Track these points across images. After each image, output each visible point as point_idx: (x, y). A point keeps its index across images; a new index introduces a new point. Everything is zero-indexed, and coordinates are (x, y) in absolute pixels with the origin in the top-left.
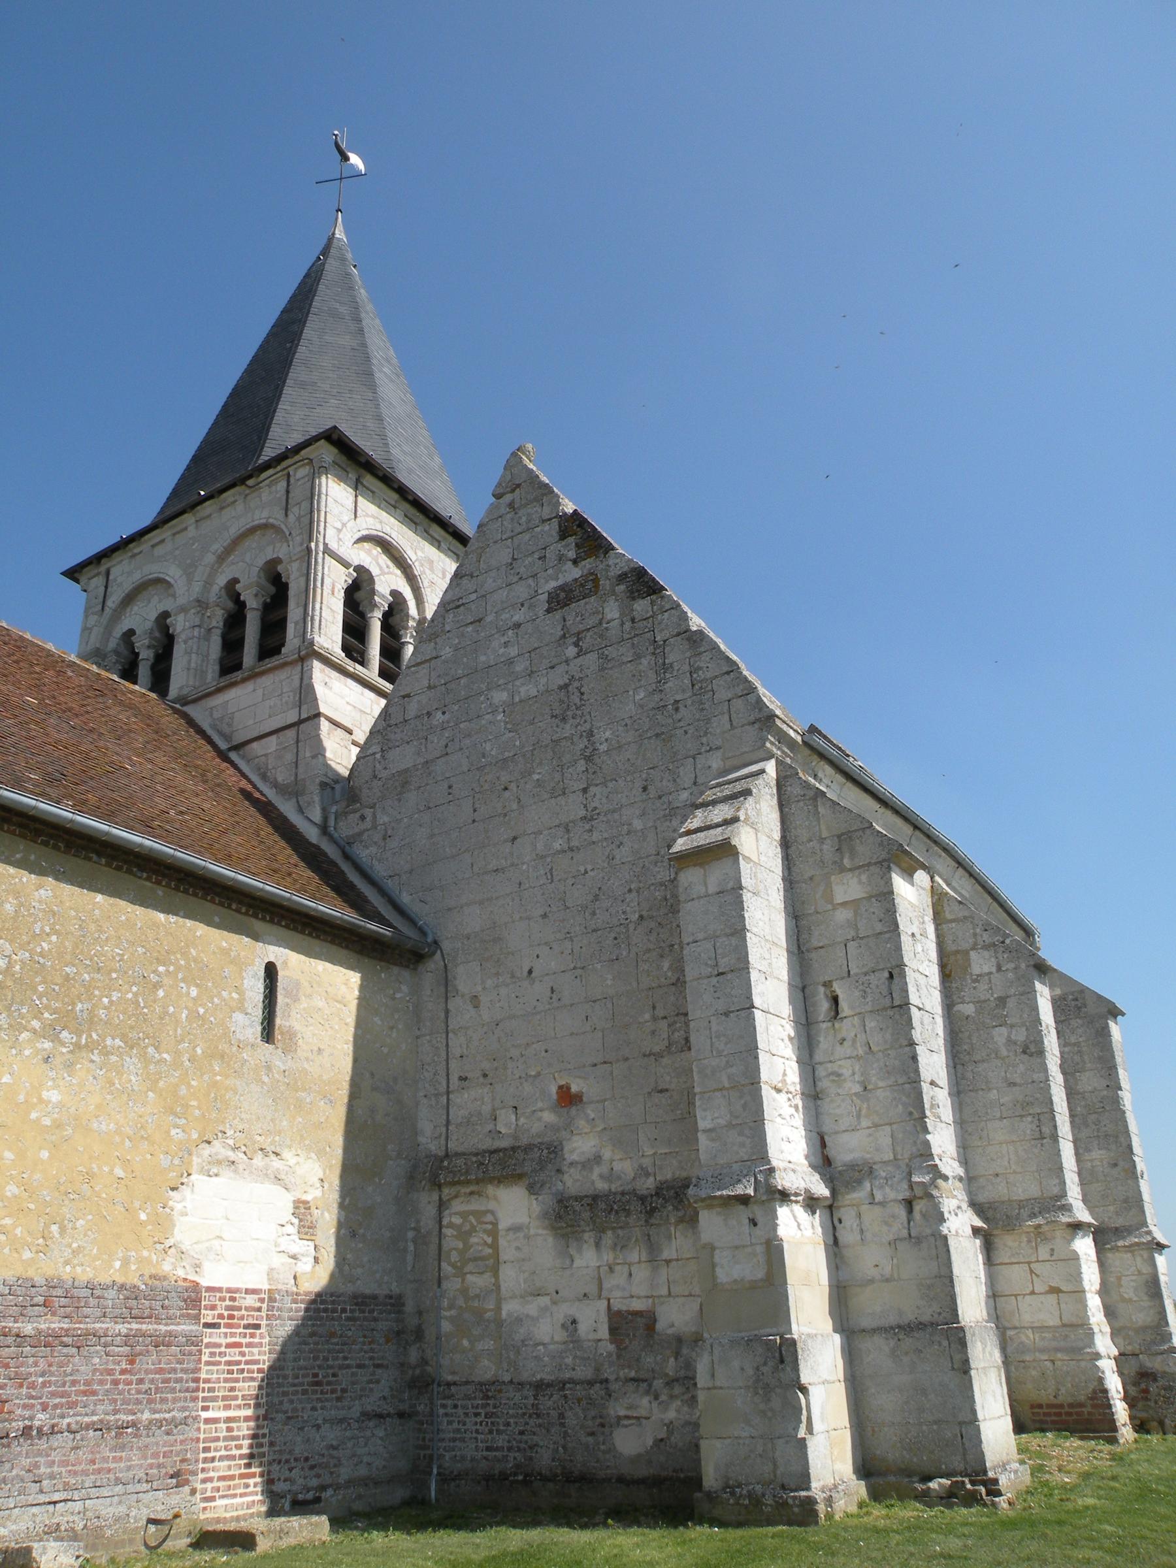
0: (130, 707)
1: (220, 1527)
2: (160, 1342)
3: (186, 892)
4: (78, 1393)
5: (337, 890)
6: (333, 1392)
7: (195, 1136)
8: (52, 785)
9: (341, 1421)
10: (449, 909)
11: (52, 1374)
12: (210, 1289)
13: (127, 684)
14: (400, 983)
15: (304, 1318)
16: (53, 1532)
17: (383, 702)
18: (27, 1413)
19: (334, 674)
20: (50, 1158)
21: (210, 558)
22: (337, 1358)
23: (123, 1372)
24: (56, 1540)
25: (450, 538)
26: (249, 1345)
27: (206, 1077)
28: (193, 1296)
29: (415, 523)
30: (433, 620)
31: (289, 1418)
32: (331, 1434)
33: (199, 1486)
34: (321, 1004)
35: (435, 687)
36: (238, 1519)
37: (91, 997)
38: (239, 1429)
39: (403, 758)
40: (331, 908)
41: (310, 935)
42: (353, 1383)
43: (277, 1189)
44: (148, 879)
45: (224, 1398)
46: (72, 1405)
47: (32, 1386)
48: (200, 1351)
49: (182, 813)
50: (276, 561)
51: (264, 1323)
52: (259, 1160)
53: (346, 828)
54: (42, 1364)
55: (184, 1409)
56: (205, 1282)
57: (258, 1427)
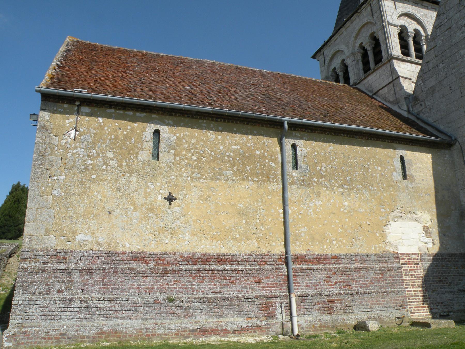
0: (341, 90)
1: (418, 321)
2: (390, 269)
3: (371, 139)
4: (369, 283)
5: (417, 129)
6: (447, 283)
7: (389, 210)
8: (326, 117)
9: (451, 292)
10: (459, 128)
11: (361, 279)
12: (401, 254)
13: (338, 84)
14: (446, 155)
15: (433, 261)
16: (370, 318)
17: (420, 67)
18: (357, 289)
19: (401, 62)
20: (349, 220)
21: (353, 39)
22: (446, 273)
23: (380, 278)
24: (371, 320)
25: (431, 4)
26: (416, 270)
27: (388, 193)
28: (397, 256)
29: (417, 4)
30: (432, 34)
31: (433, 291)
32: (449, 296)
33: (409, 309)
34: (420, 166)
35: (437, 56)
36: (423, 319)
37: (350, 175)
38: (418, 294)
39: (431, 82)
40: (424, 137)
41: (412, 145)
42: (453, 281)
43: (417, 223)
44: (359, 138)
45: (412, 285)
46: (368, 287)
47: (356, 282)
48: (402, 272)
49: (364, 117)
50: (374, 33)
51: (420, 263)
52: (409, 215)
53: (416, 110)
54: (358, 276)
55: (400, 288)
56: (399, 252)
57: (424, 293)
